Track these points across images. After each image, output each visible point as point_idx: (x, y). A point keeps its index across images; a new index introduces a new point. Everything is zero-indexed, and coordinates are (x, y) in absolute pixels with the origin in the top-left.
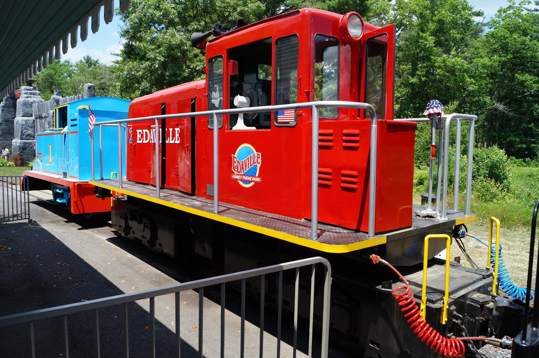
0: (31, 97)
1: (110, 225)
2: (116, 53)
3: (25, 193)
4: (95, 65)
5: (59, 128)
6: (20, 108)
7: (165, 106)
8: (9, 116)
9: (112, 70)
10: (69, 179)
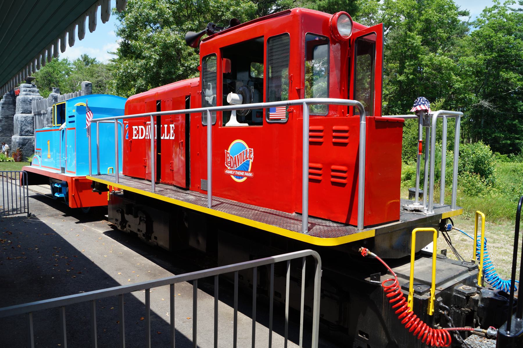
0: (30, 95)
1: (107, 219)
2: (112, 52)
3: (24, 188)
4: (92, 63)
5: (57, 124)
6: (20, 105)
8: (9, 113)
9: (108, 68)
10: (67, 174)
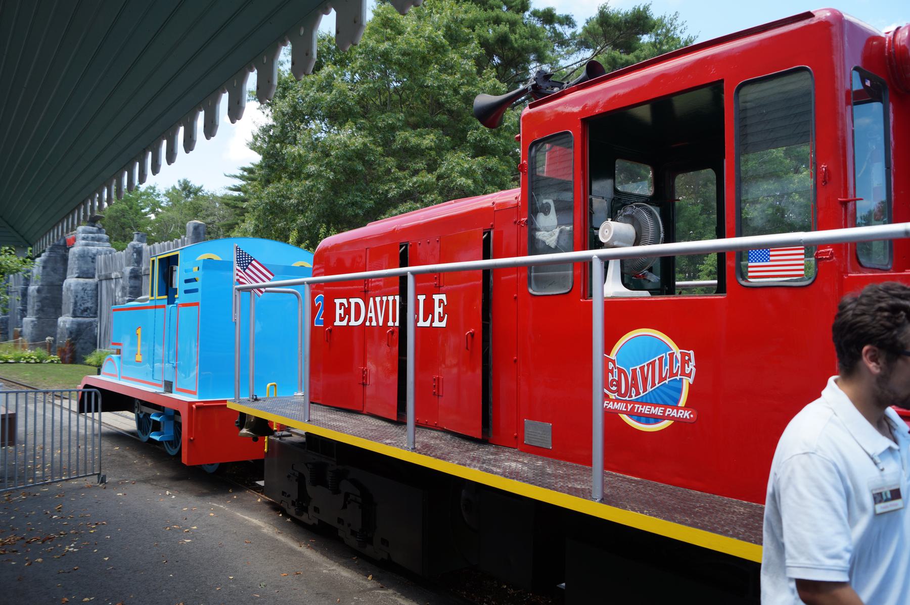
1: (259, 489)
2: (233, 174)
3: (86, 417)
4: (196, 193)
5: (159, 295)
7: (406, 248)
8: (55, 278)
9: (226, 201)
10: (176, 395)
